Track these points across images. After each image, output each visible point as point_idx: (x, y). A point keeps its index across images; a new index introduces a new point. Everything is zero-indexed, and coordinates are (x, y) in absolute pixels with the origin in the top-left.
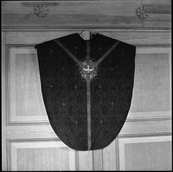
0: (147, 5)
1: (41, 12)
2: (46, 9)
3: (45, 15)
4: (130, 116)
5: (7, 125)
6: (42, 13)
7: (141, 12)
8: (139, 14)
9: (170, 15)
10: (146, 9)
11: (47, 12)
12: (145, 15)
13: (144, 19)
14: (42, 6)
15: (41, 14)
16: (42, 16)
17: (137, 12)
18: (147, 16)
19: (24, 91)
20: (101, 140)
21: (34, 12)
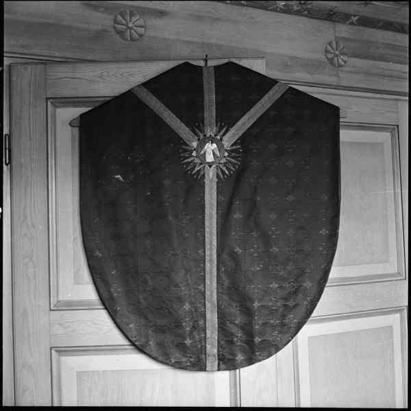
1: (131, 28)
2: (141, 22)
4: (334, 273)
5: (50, 310)
6: (133, 31)
7: (333, 52)
8: (330, 56)
9: (406, 68)
11: (143, 29)
12: (342, 60)
13: (341, 69)
14: (132, 15)
15: (130, 32)
16: (132, 40)
17: (327, 51)
18: (345, 62)
19: (34, 227)
20: (247, 344)
21: (115, 28)
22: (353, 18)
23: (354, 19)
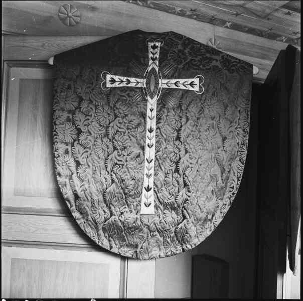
0: (220, 37)
1: (70, 17)
2: (78, 14)
3: (75, 23)
6: (71, 19)
10: (219, 44)
11: (79, 18)
15: (70, 19)
21: (59, 15)
22: (227, 23)
23: (228, 24)
